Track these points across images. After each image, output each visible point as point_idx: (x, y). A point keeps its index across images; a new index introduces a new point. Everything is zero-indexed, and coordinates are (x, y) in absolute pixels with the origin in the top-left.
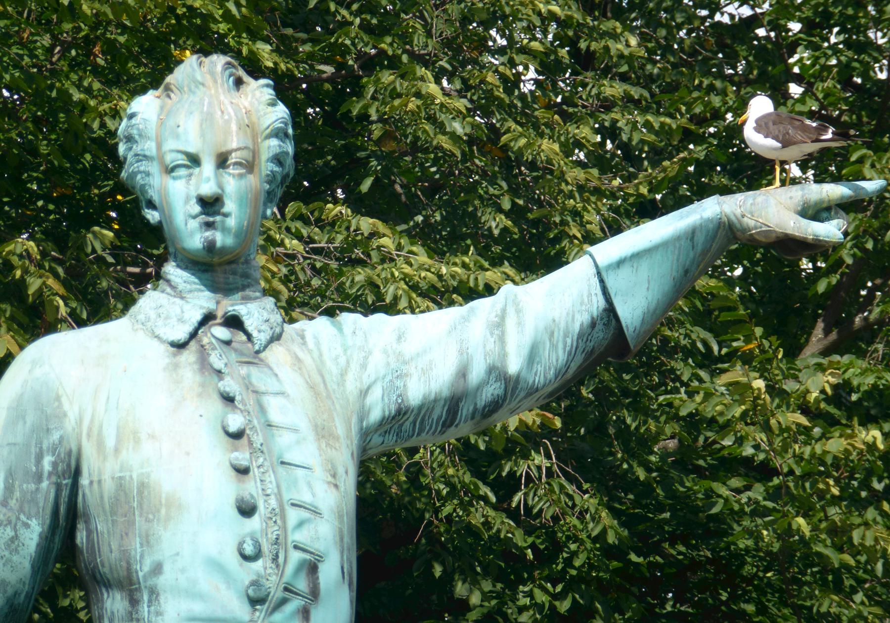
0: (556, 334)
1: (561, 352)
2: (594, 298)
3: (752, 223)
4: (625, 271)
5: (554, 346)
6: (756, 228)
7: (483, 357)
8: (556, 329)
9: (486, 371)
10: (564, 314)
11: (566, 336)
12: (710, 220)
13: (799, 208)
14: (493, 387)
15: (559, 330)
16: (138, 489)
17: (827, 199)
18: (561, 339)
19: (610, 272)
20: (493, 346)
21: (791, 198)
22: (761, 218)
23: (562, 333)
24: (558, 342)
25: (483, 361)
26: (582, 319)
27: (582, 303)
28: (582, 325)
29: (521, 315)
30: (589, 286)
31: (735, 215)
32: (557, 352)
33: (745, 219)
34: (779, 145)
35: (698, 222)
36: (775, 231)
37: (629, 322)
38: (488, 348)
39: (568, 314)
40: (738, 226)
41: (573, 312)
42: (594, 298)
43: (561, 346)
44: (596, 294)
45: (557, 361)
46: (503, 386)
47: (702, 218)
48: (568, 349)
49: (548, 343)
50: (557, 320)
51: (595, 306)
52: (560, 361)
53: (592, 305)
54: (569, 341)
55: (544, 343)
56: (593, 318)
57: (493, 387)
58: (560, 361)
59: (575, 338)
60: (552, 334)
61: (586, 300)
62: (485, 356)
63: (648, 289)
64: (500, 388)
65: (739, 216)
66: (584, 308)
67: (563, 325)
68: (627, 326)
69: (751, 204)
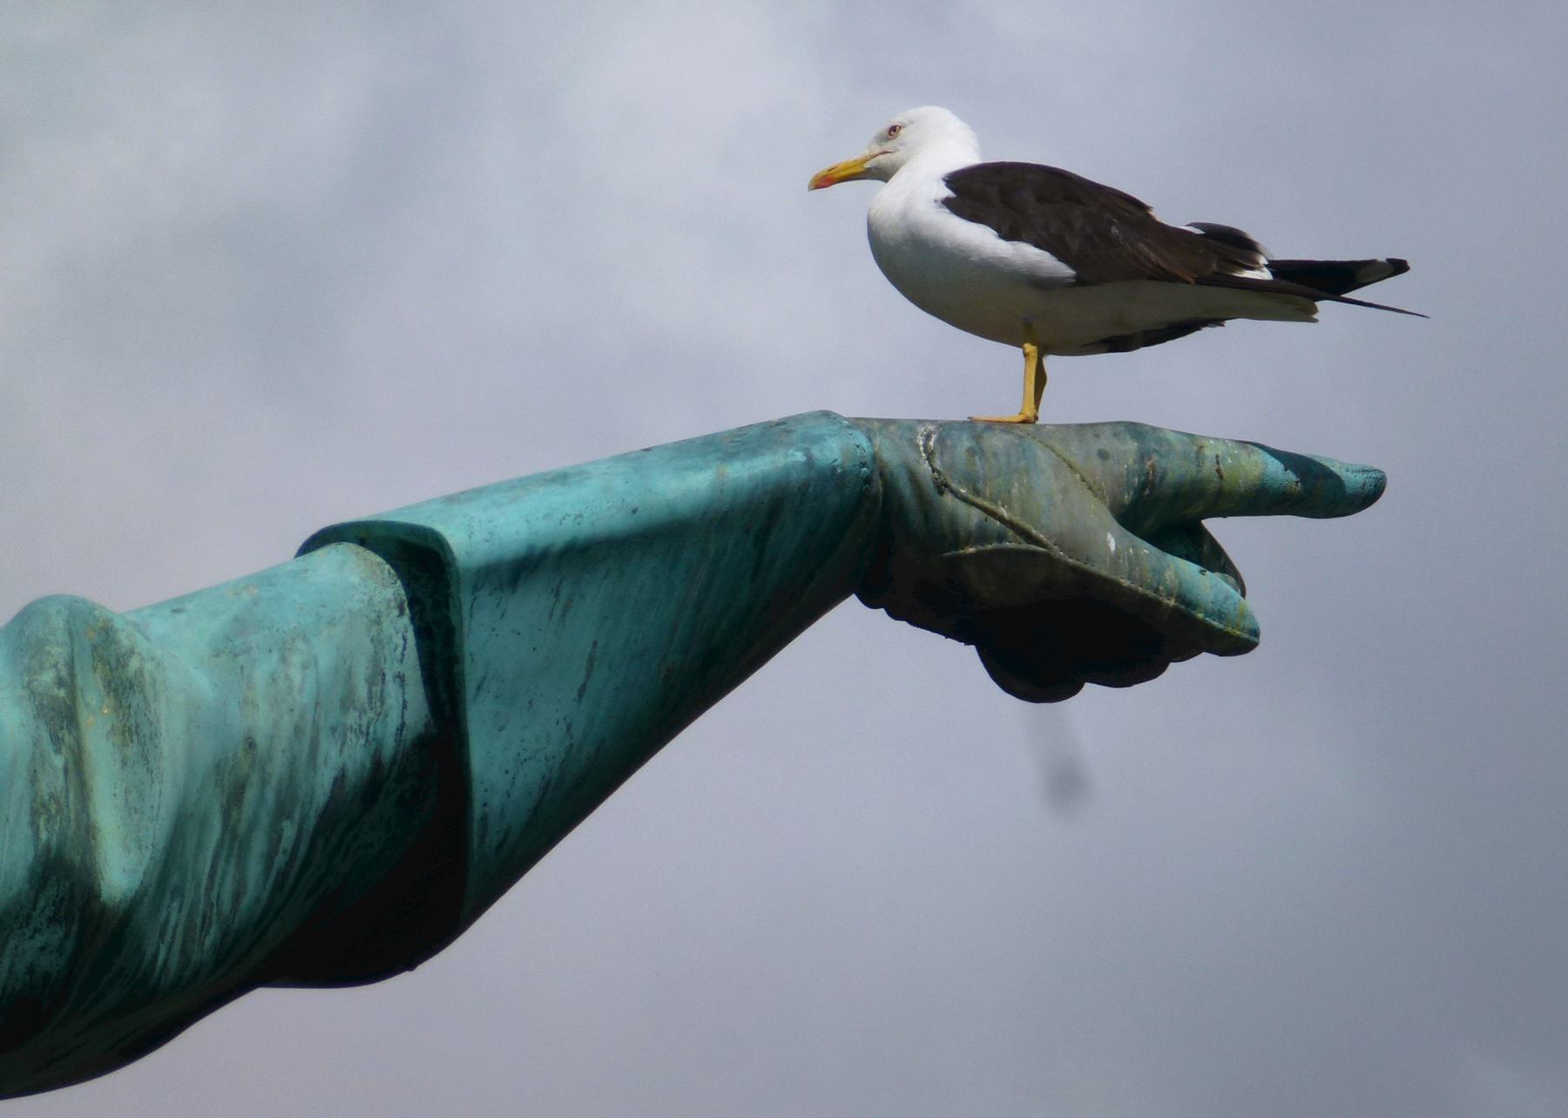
0: (250, 795)
1: (254, 868)
2: (392, 689)
3: (971, 517)
4: (529, 607)
5: (235, 842)
6: (982, 536)
7: (25, 819)
8: (255, 779)
9: (32, 871)
10: (287, 723)
11: (282, 810)
12: (833, 478)
13: (1127, 498)
14: (40, 940)
15: (264, 782)
16: (371, 683)
17: (1213, 486)
18: (265, 820)
19: (483, 594)
20: (60, 783)
21: (1103, 455)
22: (1007, 503)
23: (270, 796)
24: (253, 824)
25: (25, 830)
26: (341, 758)
27: (347, 703)
28: (340, 780)
29: (136, 700)
30: (378, 642)
31: (913, 478)
32: (241, 867)
33: (948, 499)
34: (1065, 271)
35: (797, 477)
36: (1049, 559)
37: (496, 802)
38: (44, 789)
39: (298, 731)
40: (916, 519)
41: (315, 723)
42: (392, 689)
43: (259, 844)
44: (401, 678)
45: (237, 898)
46: (70, 945)
47: (810, 462)
48: (280, 860)
49: (216, 822)
50: (260, 740)
51: (394, 721)
52: (246, 902)
53: (382, 715)
54: (289, 831)
55: (204, 823)
56: (377, 763)
57: (40, 940)
58: (246, 902)
59: (311, 823)
60: (235, 796)
61: (362, 691)
62: (34, 813)
63: (582, 691)
64: (60, 950)
65: (929, 485)
66: (352, 719)
67: (278, 767)
68: (485, 818)
69: (971, 452)
